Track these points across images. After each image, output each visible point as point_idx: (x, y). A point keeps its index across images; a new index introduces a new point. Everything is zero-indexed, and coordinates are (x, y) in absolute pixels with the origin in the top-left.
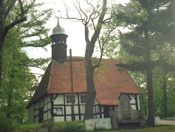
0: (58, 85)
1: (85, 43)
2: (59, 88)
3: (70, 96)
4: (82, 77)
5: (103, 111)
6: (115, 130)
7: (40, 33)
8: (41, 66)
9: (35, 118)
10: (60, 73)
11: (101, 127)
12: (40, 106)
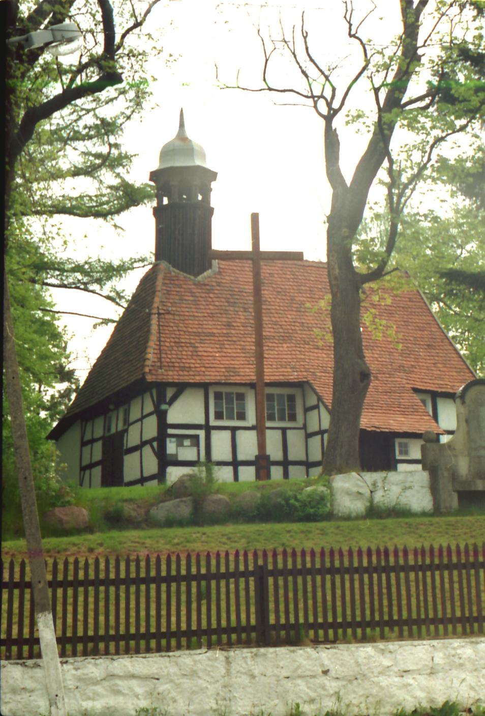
0: (184, 353)
1: (327, 192)
2: (187, 365)
4: (270, 326)
6: (448, 514)
7: (99, 167)
8: (98, 286)
9: (87, 472)
10: (187, 310)
11: (393, 503)
12: (107, 428)
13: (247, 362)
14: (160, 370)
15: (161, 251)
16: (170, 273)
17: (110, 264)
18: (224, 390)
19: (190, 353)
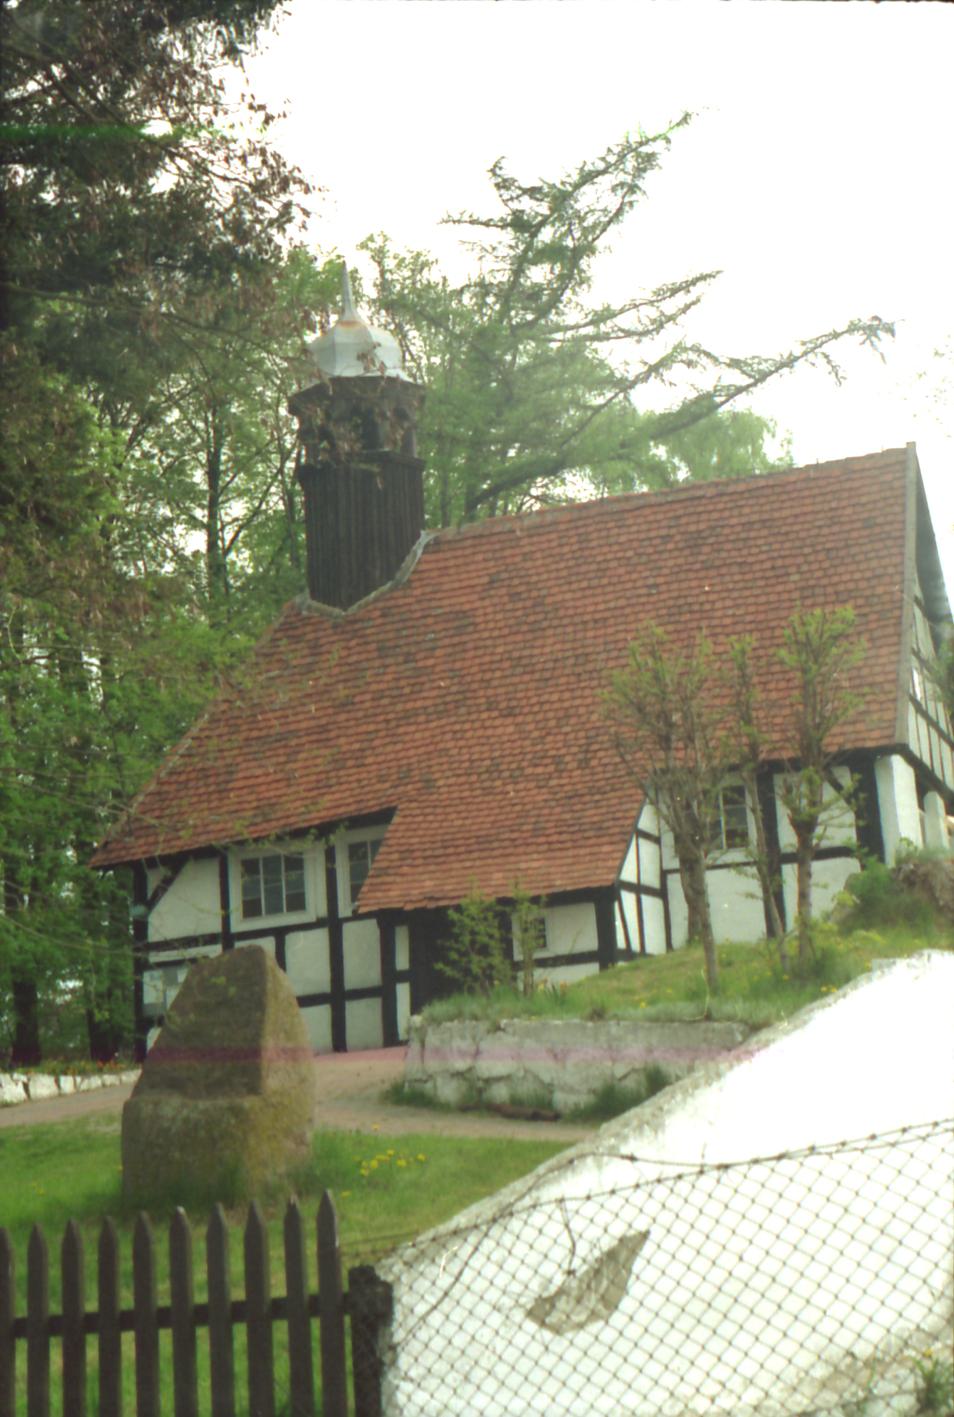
3: (266, 860)
5: (402, 962)
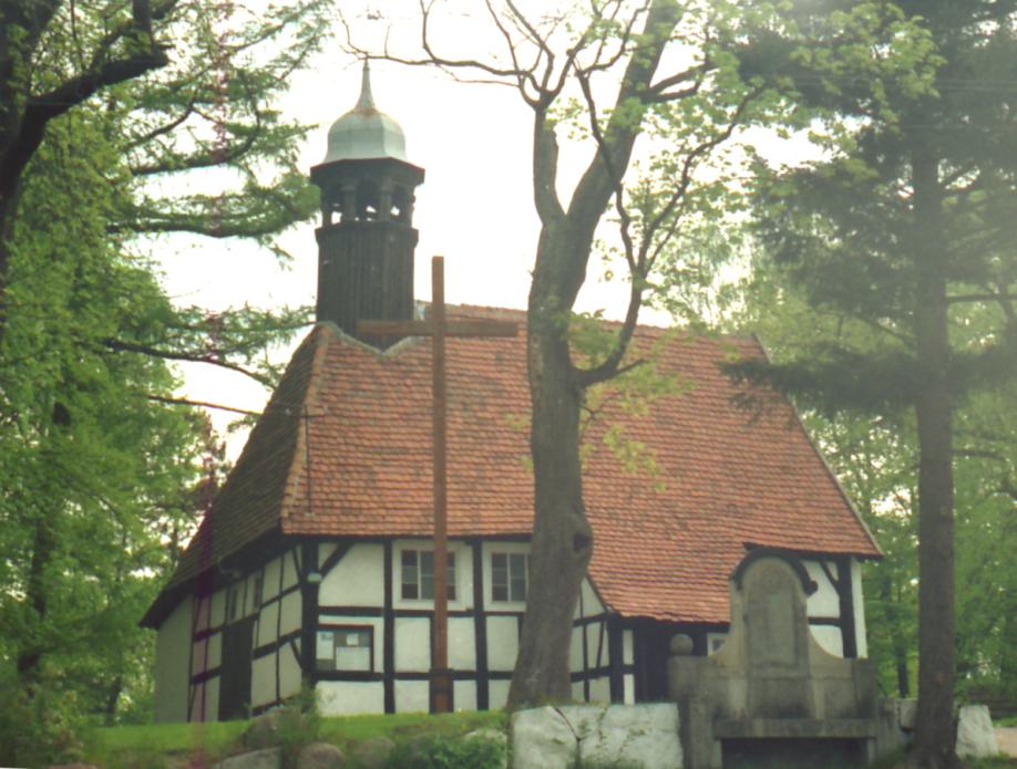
0: (353, 483)
2: (355, 505)
3: (513, 556)
4: (506, 435)
7: (246, 148)
8: (244, 358)
10: (364, 407)
11: (614, 758)
12: (230, 609)
13: (459, 500)
14: (307, 514)
15: (325, 307)
16: (339, 343)
17: (268, 315)
18: (419, 547)
19: (362, 484)
